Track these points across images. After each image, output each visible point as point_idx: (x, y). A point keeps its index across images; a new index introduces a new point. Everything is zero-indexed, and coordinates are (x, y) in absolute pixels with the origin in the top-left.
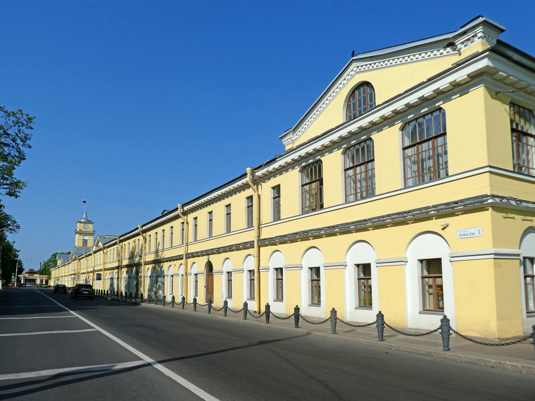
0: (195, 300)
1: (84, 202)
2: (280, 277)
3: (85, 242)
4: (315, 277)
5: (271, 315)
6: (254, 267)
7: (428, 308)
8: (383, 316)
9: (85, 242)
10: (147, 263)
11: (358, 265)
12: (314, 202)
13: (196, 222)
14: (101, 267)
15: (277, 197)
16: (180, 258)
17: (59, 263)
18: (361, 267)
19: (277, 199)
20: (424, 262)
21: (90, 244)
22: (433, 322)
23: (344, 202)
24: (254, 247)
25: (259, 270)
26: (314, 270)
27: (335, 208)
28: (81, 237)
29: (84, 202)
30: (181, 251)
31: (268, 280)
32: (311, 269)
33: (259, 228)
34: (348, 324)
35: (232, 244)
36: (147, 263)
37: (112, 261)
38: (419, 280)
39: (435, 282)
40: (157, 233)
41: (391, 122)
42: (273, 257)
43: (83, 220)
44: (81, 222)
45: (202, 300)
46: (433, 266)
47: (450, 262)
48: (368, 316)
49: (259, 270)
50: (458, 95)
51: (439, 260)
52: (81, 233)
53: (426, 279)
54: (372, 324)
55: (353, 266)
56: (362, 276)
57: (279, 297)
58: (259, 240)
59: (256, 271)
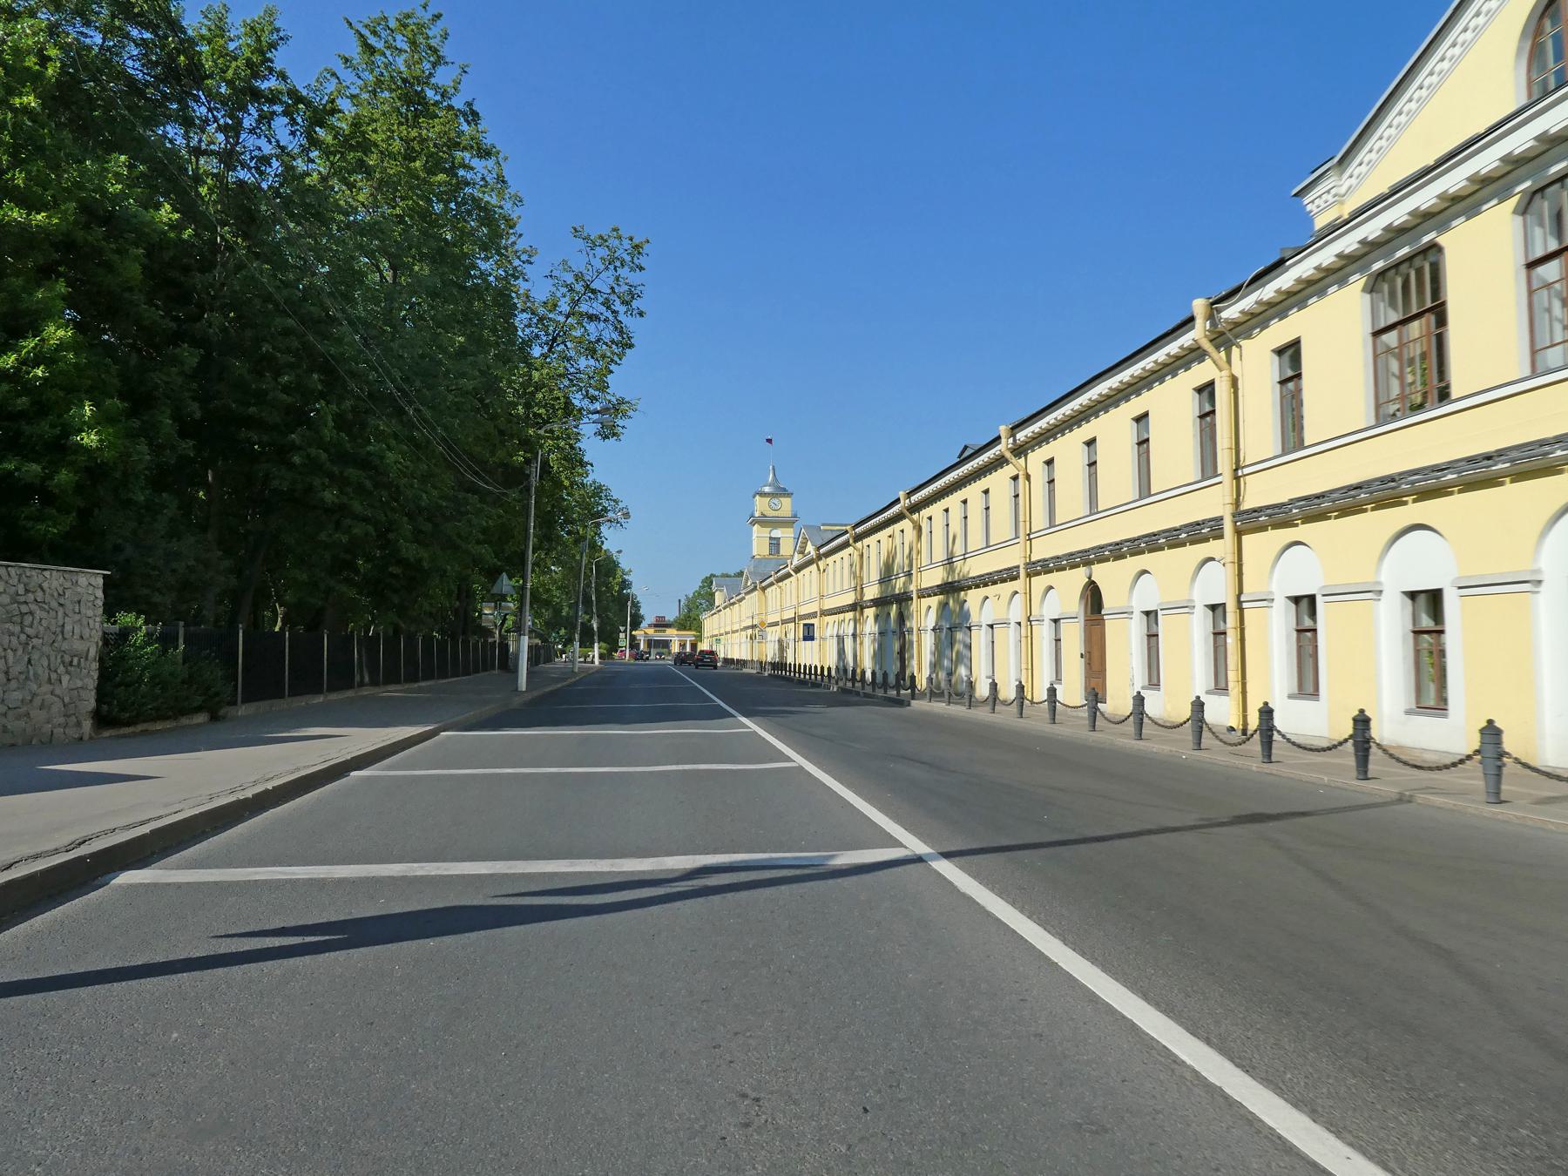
0: (1052, 692)
1: (769, 441)
2: (1308, 623)
3: (775, 544)
4: (1426, 622)
5: (1276, 736)
9: (775, 544)
10: (924, 593)
12: (1418, 375)
14: (814, 608)
15: (1207, 414)
17: (719, 598)
19: (1291, 385)
21: (786, 548)
24: (1221, 537)
25: (1239, 602)
27: (1493, 396)
28: (765, 532)
29: (769, 441)
30: (1213, 503)
33: (1237, 478)
36: (924, 593)
42: (1282, 566)
43: (767, 489)
44: (763, 494)
45: (1072, 692)
49: (1239, 602)
50: (1494, 202)
52: (764, 521)
57: (1307, 685)
58: (1238, 514)
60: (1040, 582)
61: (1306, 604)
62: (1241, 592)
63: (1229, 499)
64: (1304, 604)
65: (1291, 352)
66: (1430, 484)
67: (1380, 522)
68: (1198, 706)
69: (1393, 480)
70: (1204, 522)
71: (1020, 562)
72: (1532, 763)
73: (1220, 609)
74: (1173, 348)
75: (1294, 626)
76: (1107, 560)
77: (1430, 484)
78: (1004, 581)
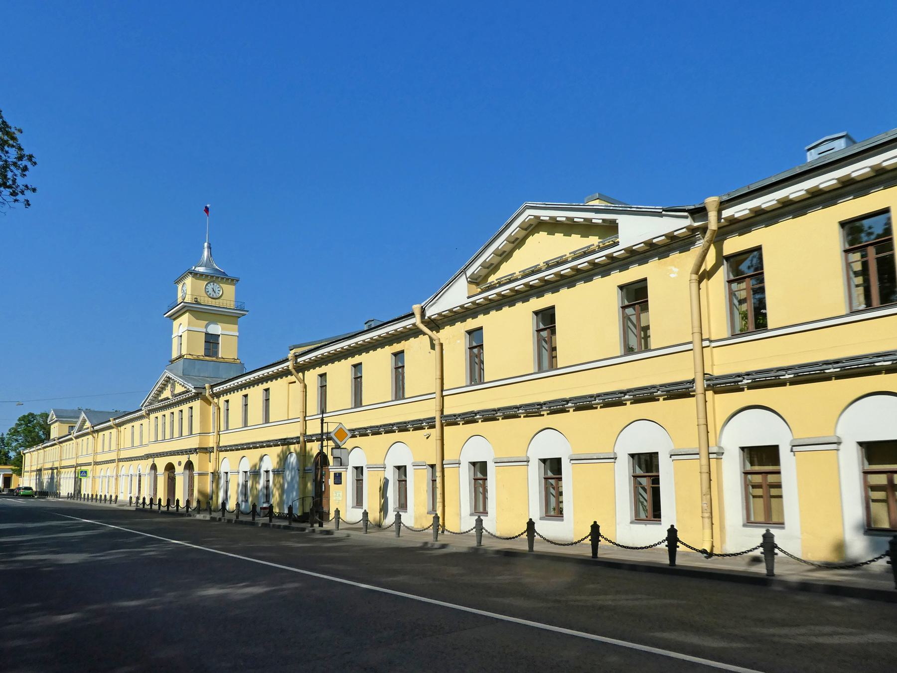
0: (398, 517)
1: (207, 210)
2: (403, 478)
3: (212, 341)
4: (479, 476)
6: (435, 460)
7: (752, 519)
8: (598, 527)
9: (212, 341)
10: (45, 469)
11: (544, 461)
12: (636, 339)
13: (246, 401)
14: (90, 460)
16: (112, 461)
18: (548, 463)
19: (476, 351)
20: (548, 463)
21: (227, 350)
22: (655, 534)
23: (537, 371)
25: (443, 465)
26: (478, 466)
28: (201, 326)
29: (207, 210)
30: (113, 456)
31: (460, 483)
32: (474, 464)
33: (443, 397)
34: (552, 542)
35: (392, 422)
36: (45, 469)
37: (84, 453)
38: (630, 479)
39: (765, 479)
40: (191, 408)
41: (663, 252)
42: (469, 445)
43: (201, 269)
44: (196, 275)
46: (554, 466)
47: (792, 451)
48: (653, 535)
49: (443, 465)
51: (775, 448)
52: (196, 310)
53: (749, 476)
54: (659, 543)
55: (627, 456)
56: (550, 474)
57: (555, 512)
58: (218, 447)
59: (438, 468)
60: (121, 464)
61: (480, 467)
62: (443, 459)
63: (438, 408)
64: (359, 470)
65: (323, 376)
66: (558, 407)
67: (385, 439)
68: (531, 524)
69: (739, 376)
70: (499, 409)
71: (116, 458)
72: (631, 545)
73: (359, 470)
74: (280, 367)
75: (543, 476)
76: (394, 432)
77: (558, 407)
78: (237, 450)
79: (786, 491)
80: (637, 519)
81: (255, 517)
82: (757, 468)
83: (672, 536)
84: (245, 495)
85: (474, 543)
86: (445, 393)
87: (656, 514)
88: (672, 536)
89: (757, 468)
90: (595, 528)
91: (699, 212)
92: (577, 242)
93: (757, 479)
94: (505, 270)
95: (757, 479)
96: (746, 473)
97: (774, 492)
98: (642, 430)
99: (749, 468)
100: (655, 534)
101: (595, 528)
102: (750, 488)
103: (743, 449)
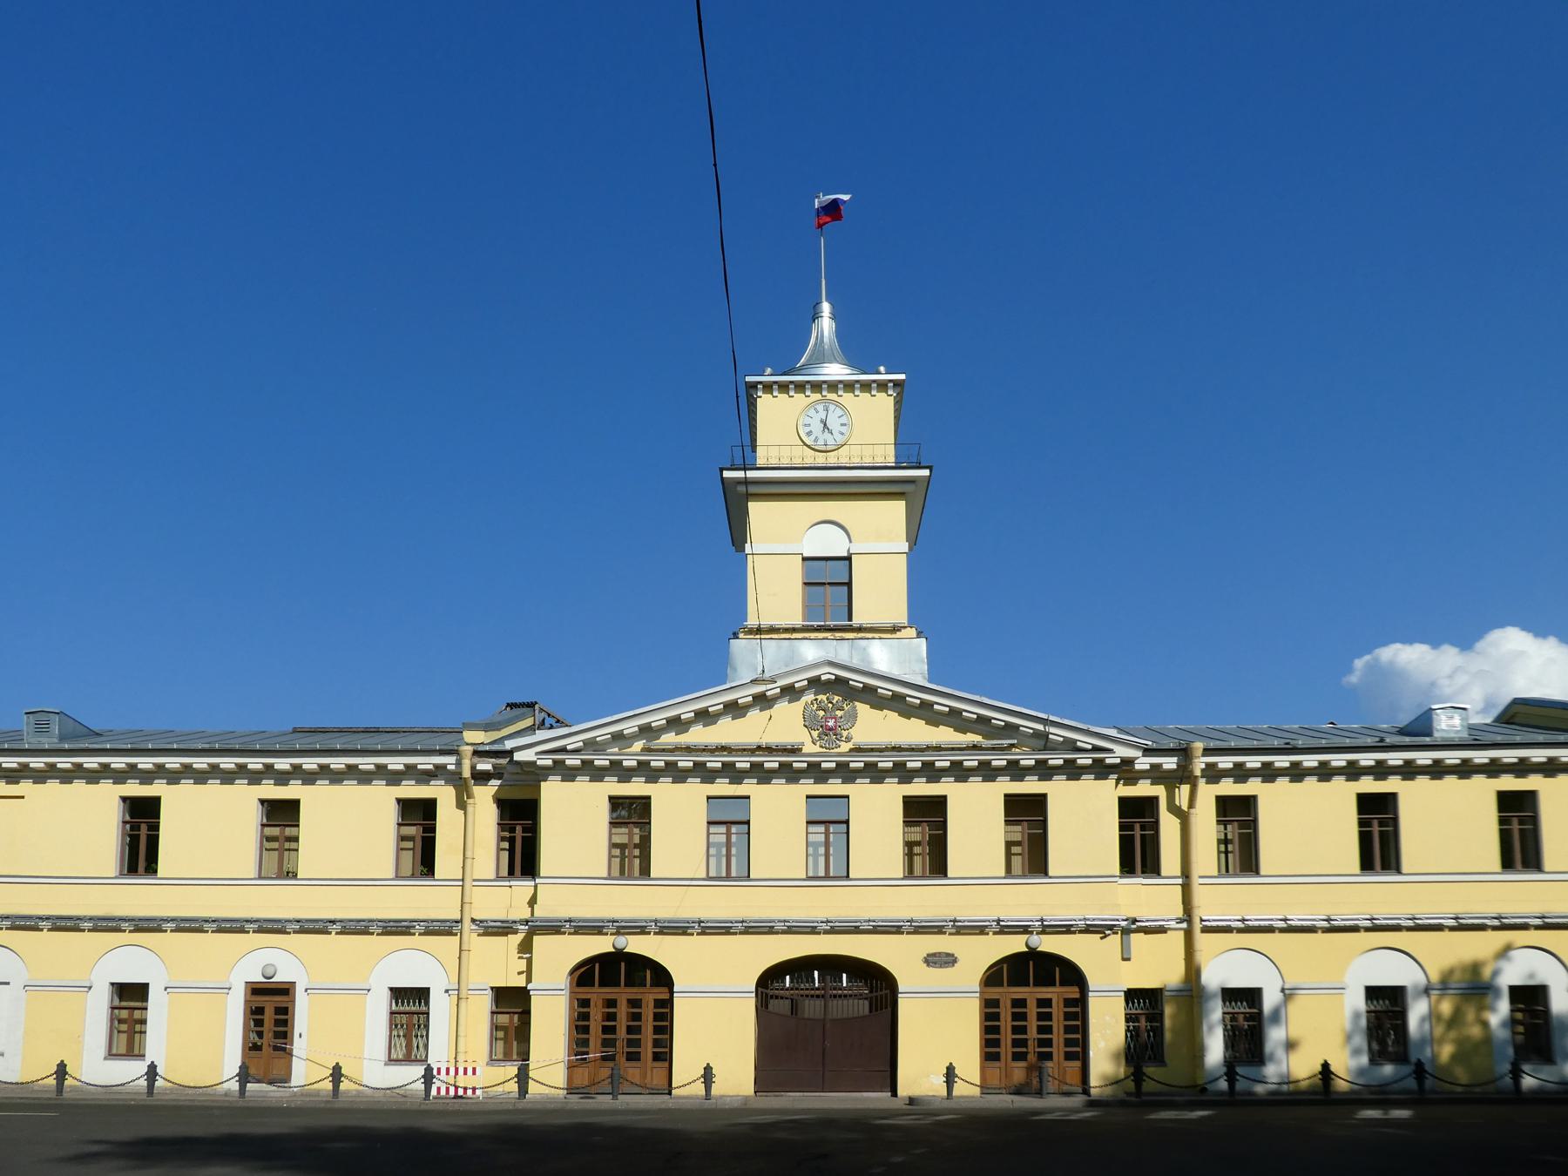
22: (410, 1075)
66: (147, 926)
79: (150, 1027)
80: (111, 1055)
81: (1311, 1091)
82: (124, 1004)
83: (152, 1072)
84: (259, 1023)
85: (54, 1095)
86: (1180, 881)
87: (133, 1051)
88: (152, 1072)
89: (124, 1004)
90: (708, 1069)
91: (1184, 753)
92: (945, 735)
93: (124, 1014)
94: (698, 735)
95: (124, 1014)
96: (113, 1008)
97: (138, 1027)
98: (413, 963)
99: (117, 1003)
100: (140, 1068)
101: (708, 1069)
102: (115, 1022)
103: (391, 989)
